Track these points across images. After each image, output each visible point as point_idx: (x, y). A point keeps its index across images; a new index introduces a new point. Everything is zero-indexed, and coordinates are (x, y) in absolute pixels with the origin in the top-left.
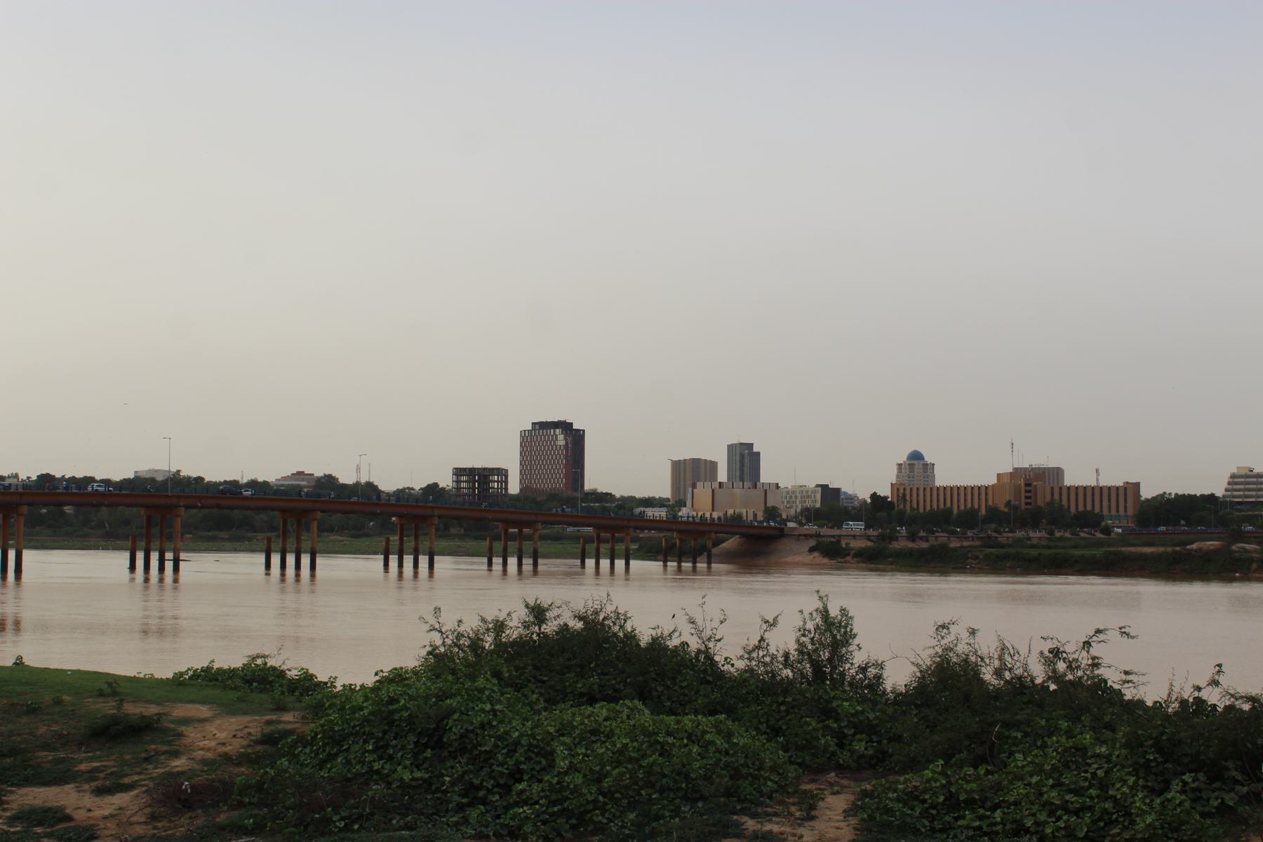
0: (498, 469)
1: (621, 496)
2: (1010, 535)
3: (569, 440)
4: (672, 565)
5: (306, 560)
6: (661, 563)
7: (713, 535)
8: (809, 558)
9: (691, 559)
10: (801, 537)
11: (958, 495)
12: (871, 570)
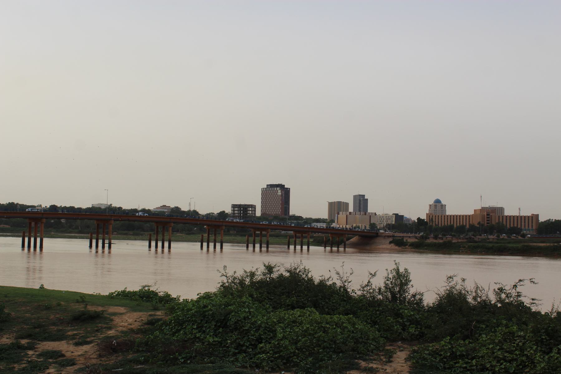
0: (251, 205)
2: (480, 237)
3: (283, 192)
4: (328, 249)
5: (166, 244)
7: (347, 236)
8: (389, 246)
9: (337, 246)
10: (386, 237)
11: (460, 219)
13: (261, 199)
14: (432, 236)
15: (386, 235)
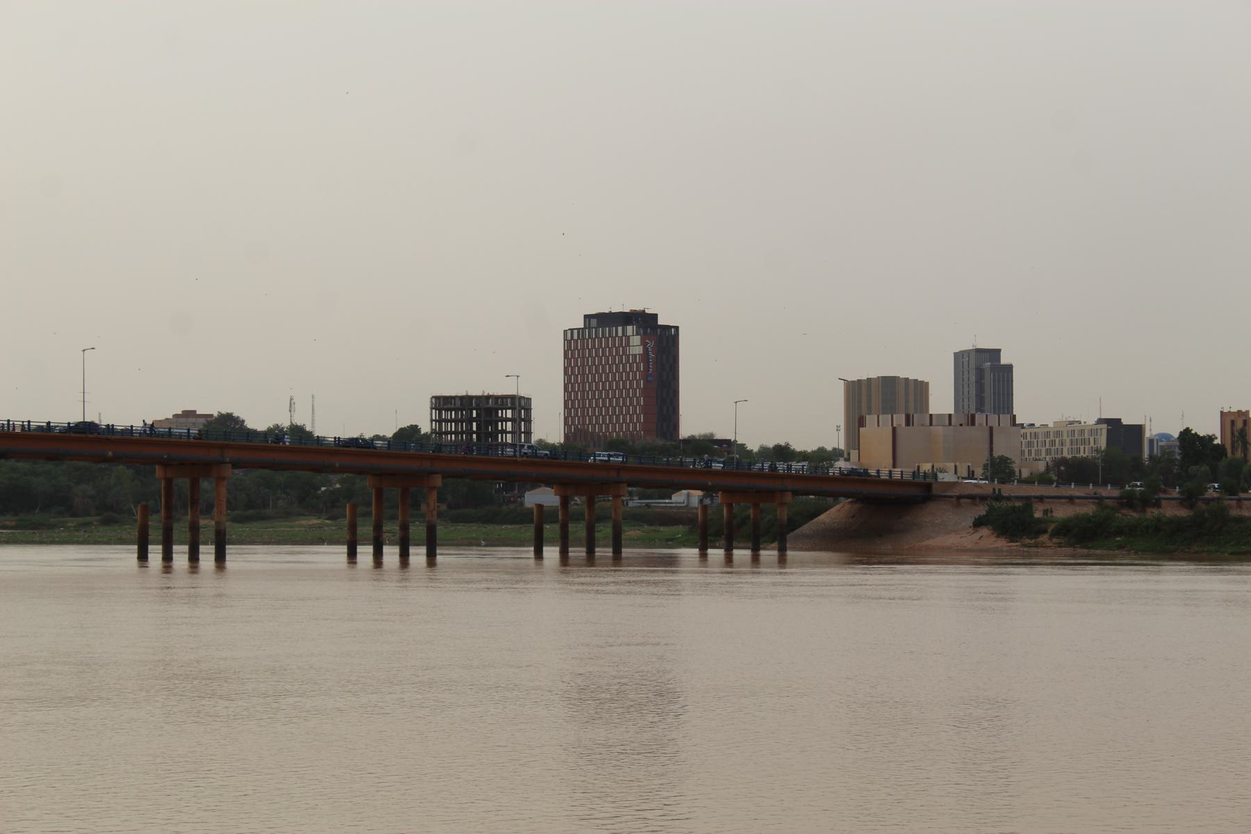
0: (513, 397)
3: (651, 344)
4: (716, 554)
7: (789, 498)
8: (969, 539)
9: (750, 545)
10: (962, 501)
12: (1088, 556)
14: (1176, 492)
15: (967, 492)
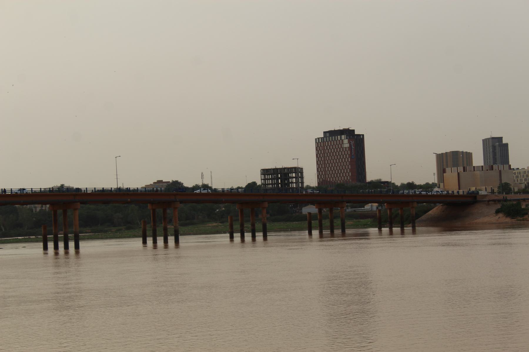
0: (295, 168)
1: (157, 181)
3: (352, 143)
4: (385, 230)
5: (72, 244)
6: (377, 229)
7: (415, 205)
8: (494, 219)
9: (400, 225)
10: (490, 202)
13: (317, 157)
